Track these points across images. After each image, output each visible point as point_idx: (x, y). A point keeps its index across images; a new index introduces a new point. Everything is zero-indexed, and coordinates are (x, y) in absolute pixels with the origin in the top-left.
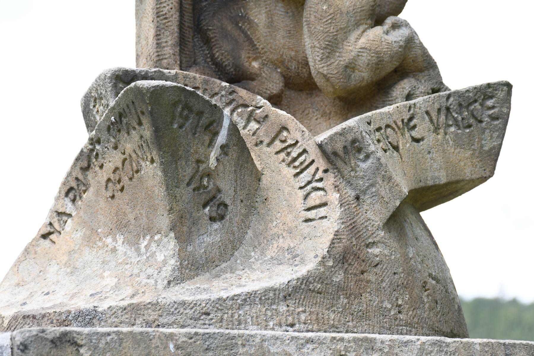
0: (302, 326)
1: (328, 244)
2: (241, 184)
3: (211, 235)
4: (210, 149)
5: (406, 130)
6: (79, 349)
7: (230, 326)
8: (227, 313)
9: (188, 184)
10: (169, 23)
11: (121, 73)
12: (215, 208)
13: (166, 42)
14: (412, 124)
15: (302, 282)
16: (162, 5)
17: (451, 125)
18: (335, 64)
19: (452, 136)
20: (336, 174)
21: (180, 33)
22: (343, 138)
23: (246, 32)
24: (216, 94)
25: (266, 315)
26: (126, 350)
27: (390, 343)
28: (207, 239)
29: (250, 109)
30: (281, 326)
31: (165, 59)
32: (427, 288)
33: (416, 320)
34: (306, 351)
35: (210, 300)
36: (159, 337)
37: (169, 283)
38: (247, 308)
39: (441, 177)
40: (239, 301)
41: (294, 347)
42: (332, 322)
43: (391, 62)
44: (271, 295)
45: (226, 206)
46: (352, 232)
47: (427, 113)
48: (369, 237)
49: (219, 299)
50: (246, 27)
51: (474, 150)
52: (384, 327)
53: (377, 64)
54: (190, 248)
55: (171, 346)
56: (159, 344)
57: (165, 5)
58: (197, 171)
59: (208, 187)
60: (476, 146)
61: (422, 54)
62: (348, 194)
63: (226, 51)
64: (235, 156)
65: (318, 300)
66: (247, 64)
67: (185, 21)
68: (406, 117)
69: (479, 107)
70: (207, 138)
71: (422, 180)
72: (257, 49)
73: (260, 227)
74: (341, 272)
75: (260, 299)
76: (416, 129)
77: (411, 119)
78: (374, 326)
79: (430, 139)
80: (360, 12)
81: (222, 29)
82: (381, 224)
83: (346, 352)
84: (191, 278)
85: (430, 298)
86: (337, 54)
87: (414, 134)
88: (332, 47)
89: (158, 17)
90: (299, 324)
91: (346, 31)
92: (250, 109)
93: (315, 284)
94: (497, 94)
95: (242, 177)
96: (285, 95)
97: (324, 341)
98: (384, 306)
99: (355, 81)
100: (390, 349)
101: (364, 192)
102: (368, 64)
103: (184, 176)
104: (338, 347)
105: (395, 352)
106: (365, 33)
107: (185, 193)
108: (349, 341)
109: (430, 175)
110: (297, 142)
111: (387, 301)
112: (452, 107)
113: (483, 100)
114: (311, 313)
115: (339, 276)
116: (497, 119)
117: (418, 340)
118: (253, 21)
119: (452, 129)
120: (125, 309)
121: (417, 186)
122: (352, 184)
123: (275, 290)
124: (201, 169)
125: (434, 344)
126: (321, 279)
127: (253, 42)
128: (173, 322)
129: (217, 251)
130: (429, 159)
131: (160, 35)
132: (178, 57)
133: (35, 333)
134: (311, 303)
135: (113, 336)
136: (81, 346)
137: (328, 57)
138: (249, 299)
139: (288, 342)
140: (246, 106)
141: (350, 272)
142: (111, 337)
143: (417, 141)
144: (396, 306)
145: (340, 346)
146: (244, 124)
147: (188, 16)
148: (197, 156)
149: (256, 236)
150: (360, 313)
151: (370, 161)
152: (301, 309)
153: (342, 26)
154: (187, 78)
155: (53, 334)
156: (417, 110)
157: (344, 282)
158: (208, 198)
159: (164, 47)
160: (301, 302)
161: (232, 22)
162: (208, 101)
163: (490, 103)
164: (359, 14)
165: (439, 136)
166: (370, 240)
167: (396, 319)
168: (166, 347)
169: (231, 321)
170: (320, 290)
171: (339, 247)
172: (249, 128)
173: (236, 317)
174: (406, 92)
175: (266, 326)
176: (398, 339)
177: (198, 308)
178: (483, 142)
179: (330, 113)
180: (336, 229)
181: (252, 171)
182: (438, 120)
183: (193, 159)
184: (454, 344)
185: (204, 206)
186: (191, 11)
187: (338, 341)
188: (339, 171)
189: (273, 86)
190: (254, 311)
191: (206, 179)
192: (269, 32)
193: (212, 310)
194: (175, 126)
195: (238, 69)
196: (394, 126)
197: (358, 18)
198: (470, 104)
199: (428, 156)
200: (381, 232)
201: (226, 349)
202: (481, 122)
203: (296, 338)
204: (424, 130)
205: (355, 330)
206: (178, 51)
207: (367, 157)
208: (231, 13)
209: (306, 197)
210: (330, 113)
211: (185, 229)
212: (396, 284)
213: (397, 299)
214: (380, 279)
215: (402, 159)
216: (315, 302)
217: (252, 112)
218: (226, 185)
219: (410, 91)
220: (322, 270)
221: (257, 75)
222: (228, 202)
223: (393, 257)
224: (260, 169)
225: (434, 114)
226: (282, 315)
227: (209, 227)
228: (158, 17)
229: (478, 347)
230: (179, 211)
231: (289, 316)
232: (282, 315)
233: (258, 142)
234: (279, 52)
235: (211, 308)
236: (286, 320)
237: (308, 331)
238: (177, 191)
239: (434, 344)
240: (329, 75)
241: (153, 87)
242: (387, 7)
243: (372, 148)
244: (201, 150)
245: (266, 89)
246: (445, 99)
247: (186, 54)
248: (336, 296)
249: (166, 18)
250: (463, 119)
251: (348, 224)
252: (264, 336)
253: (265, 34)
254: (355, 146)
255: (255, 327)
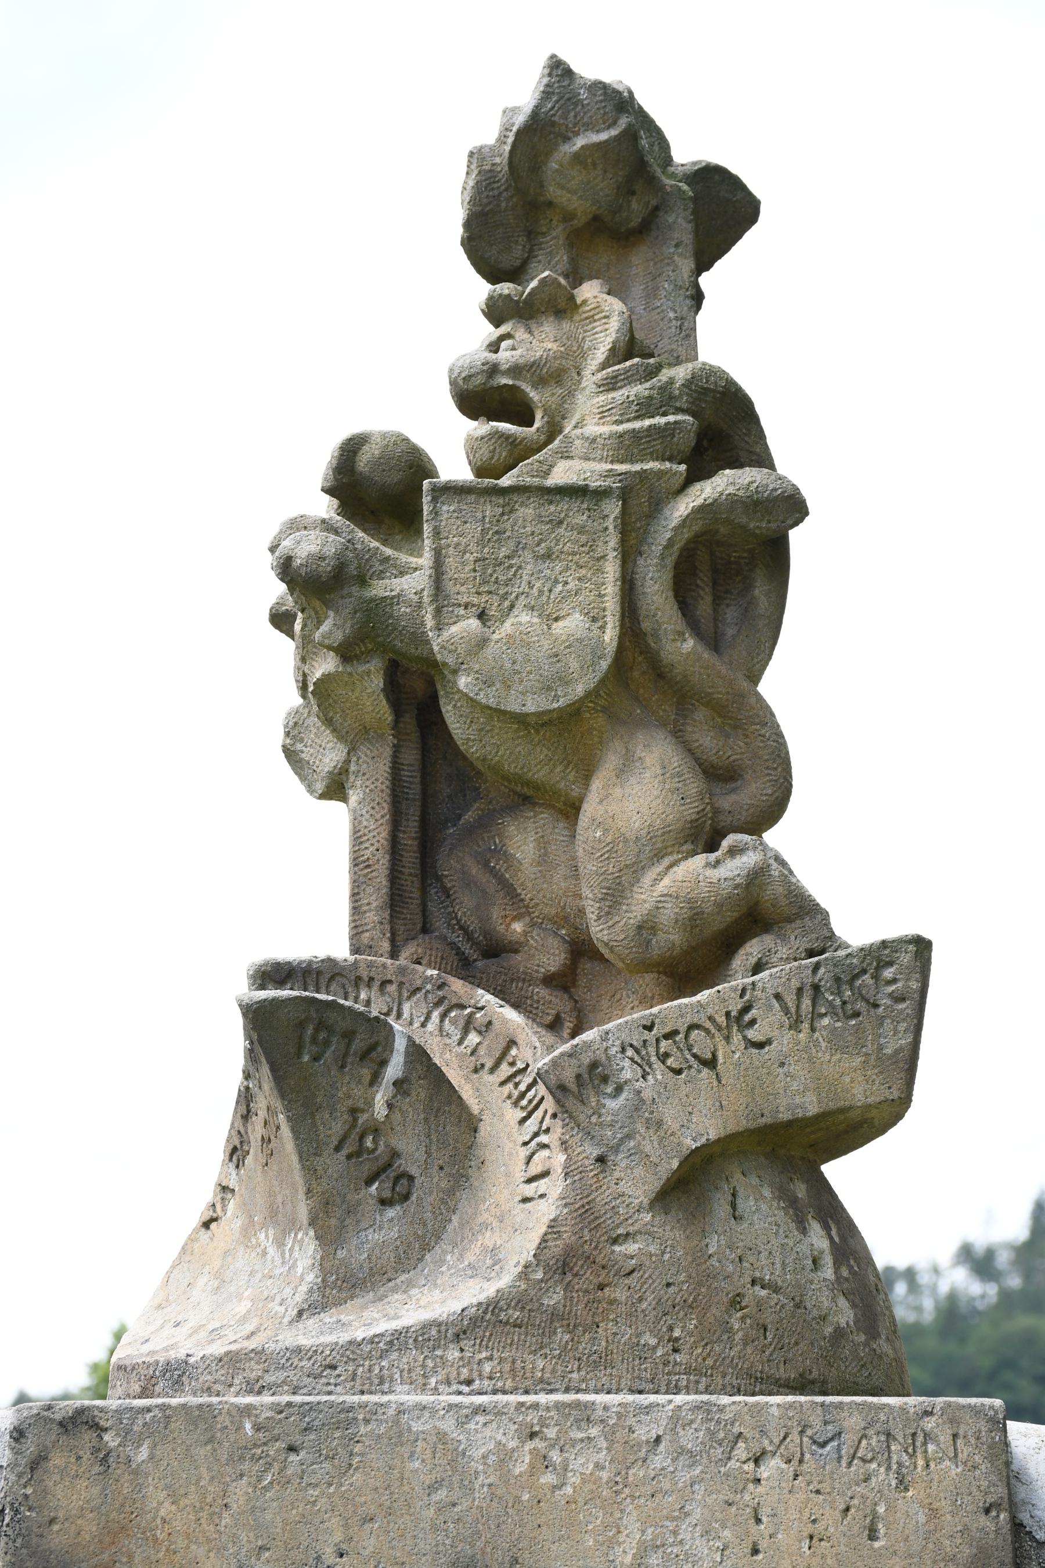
0: (486, 1382)
1: (537, 1241)
2: (438, 1141)
3: (381, 1228)
4: (375, 1088)
5: (735, 1028)
6: (103, 1434)
7: (366, 1387)
8: (363, 1365)
9: (337, 1149)
10: (374, 874)
11: (269, 968)
12: (389, 1184)
13: (369, 904)
14: (747, 1018)
15: (487, 1309)
16: (363, 846)
17: (825, 1015)
18: (622, 923)
19: (825, 1033)
20: (567, 1120)
21: (391, 888)
22: (574, 1061)
23: (503, 875)
24: (418, 989)
25: (424, 1366)
26: (176, 1435)
27: (619, 1409)
28: (374, 1237)
29: (469, 1010)
30: (449, 1383)
31: (367, 931)
32: (743, 1304)
33: (710, 1362)
34: (473, 1427)
35: (337, 1344)
36: (229, 1412)
37: (300, 1313)
38: (394, 1355)
39: (807, 1105)
40: (381, 1345)
41: (453, 1421)
42: (540, 1375)
43: (718, 913)
44: (434, 1332)
45: (411, 1178)
46: (584, 1219)
47: (778, 997)
48: (618, 1226)
49: (350, 1342)
50: (501, 866)
51: (866, 1054)
52: (641, 1379)
53: (691, 919)
54: (341, 1254)
55: (248, 1426)
56: (228, 1423)
57: (367, 845)
58: (353, 1125)
59: (376, 1149)
60: (870, 1048)
61: (786, 892)
62: (584, 1155)
63: (468, 909)
64: (423, 1095)
65: (516, 1338)
66: (501, 928)
67: (403, 866)
68: (735, 1007)
69: (871, 982)
70: (366, 1073)
71: (766, 1112)
72: (522, 900)
73: (470, 1211)
74: (558, 1290)
75: (415, 1340)
76: (756, 1026)
77: (747, 1009)
78: (620, 1377)
79: (784, 1041)
80: (662, 835)
81: (464, 873)
82: (646, 1201)
83: (542, 1426)
84: (340, 1303)
85: (748, 1321)
86: (624, 907)
87: (752, 1034)
88: (615, 896)
89: (356, 865)
90: (480, 1379)
91: (637, 869)
92: (469, 1010)
93: (511, 1312)
94: (898, 958)
95: (441, 1129)
96: (584, 970)
97: (505, 1410)
98: (642, 1342)
99: (659, 949)
100: (619, 1418)
101: (616, 1149)
102: (676, 921)
103: (329, 1136)
104: (529, 1419)
105: (628, 1423)
106: (672, 871)
107: (334, 1163)
108: (548, 1409)
109: (783, 1102)
110: (528, 1065)
111: (648, 1333)
112: (823, 983)
113: (877, 968)
114: (501, 1360)
115: (555, 1296)
116: (903, 999)
117: (670, 1401)
118: (513, 856)
119: (826, 1021)
120: (220, 1360)
121: (752, 1125)
122: (593, 1137)
123: (440, 1325)
124: (360, 1121)
125: (697, 1407)
126: (520, 1301)
127: (515, 889)
128: (283, 1382)
129: (392, 1255)
130: (782, 1076)
131: (358, 894)
132: (388, 927)
133: (35, 1411)
134: (502, 1344)
135: (156, 1412)
136: (106, 1429)
137: (608, 913)
138: (398, 1340)
139: (442, 1412)
140: (463, 1007)
141: (576, 1287)
142: (152, 1414)
143: (760, 1045)
144: (669, 1341)
145: (532, 1417)
146: (459, 1037)
147: (410, 859)
148: (350, 1102)
149: (462, 1225)
150: (595, 1357)
151: (624, 1095)
152: (484, 1355)
153: (628, 862)
154: (373, 966)
155: (63, 1411)
156: (758, 993)
157: (565, 1306)
158: (375, 1168)
159: (365, 912)
160: (484, 1343)
161: (478, 862)
162: (361, 1013)
163: (888, 973)
164: (659, 839)
165: (801, 1035)
166: (620, 1231)
167: (666, 1364)
168: (240, 1428)
169: (369, 1378)
170: (519, 1321)
171: (556, 1246)
172: (466, 1043)
173: (376, 1372)
174: (753, 960)
175: (425, 1385)
176: (634, 1402)
177: (319, 1358)
178: (882, 1041)
179: (653, 998)
180: (552, 1217)
181: (460, 1117)
182: (798, 1007)
183: (342, 1108)
184: (733, 1407)
185: (369, 1182)
186: (415, 848)
187: (528, 1408)
188: (571, 1117)
189: (548, 959)
190: (405, 1360)
191: (371, 1138)
192: (540, 871)
193: (340, 1361)
194: (306, 1058)
195: (488, 937)
196: (708, 1024)
197: (659, 845)
198: (856, 977)
199: (780, 1070)
200: (645, 1215)
201: (338, 1428)
202: (876, 1006)
203: (456, 1405)
204: (771, 1026)
205: (584, 1386)
206: (388, 917)
207: (619, 1090)
208: (479, 846)
209: (529, 1160)
210: (653, 998)
211: (333, 1222)
212: (669, 1303)
213: (671, 1329)
214: (637, 1297)
215: (719, 1082)
216: (509, 1341)
217: (471, 1015)
218: (410, 1146)
219: (760, 959)
220: (523, 1287)
221: (520, 944)
222: (414, 1171)
223: (667, 1256)
224: (476, 1112)
225: (790, 1000)
226: (452, 1366)
227: (378, 1217)
228: (356, 865)
229: (775, 1411)
230: (323, 1193)
231: (463, 1366)
232: (452, 1366)
233: (479, 1066)
234: (559, 903)
235: (338, 1357)
236: (458, 1374)
237: (495, 1392)
238: (319, 1162)
239: (698, 1408)
240: (611, 944)
241: (257, 1003)
242: (744, 813)
243: (627, 1074)
244: (358, 1092)
245: (538, 966)
246: (810, 972)
247: (405, 919)
248: (547, 1330)
249: (368, 866)
250: (844, 1003)
251: (577, 1206)
252: (402, 1404)
253: (533, 876)
254: (595, 1075)
255: (406, 1387)
